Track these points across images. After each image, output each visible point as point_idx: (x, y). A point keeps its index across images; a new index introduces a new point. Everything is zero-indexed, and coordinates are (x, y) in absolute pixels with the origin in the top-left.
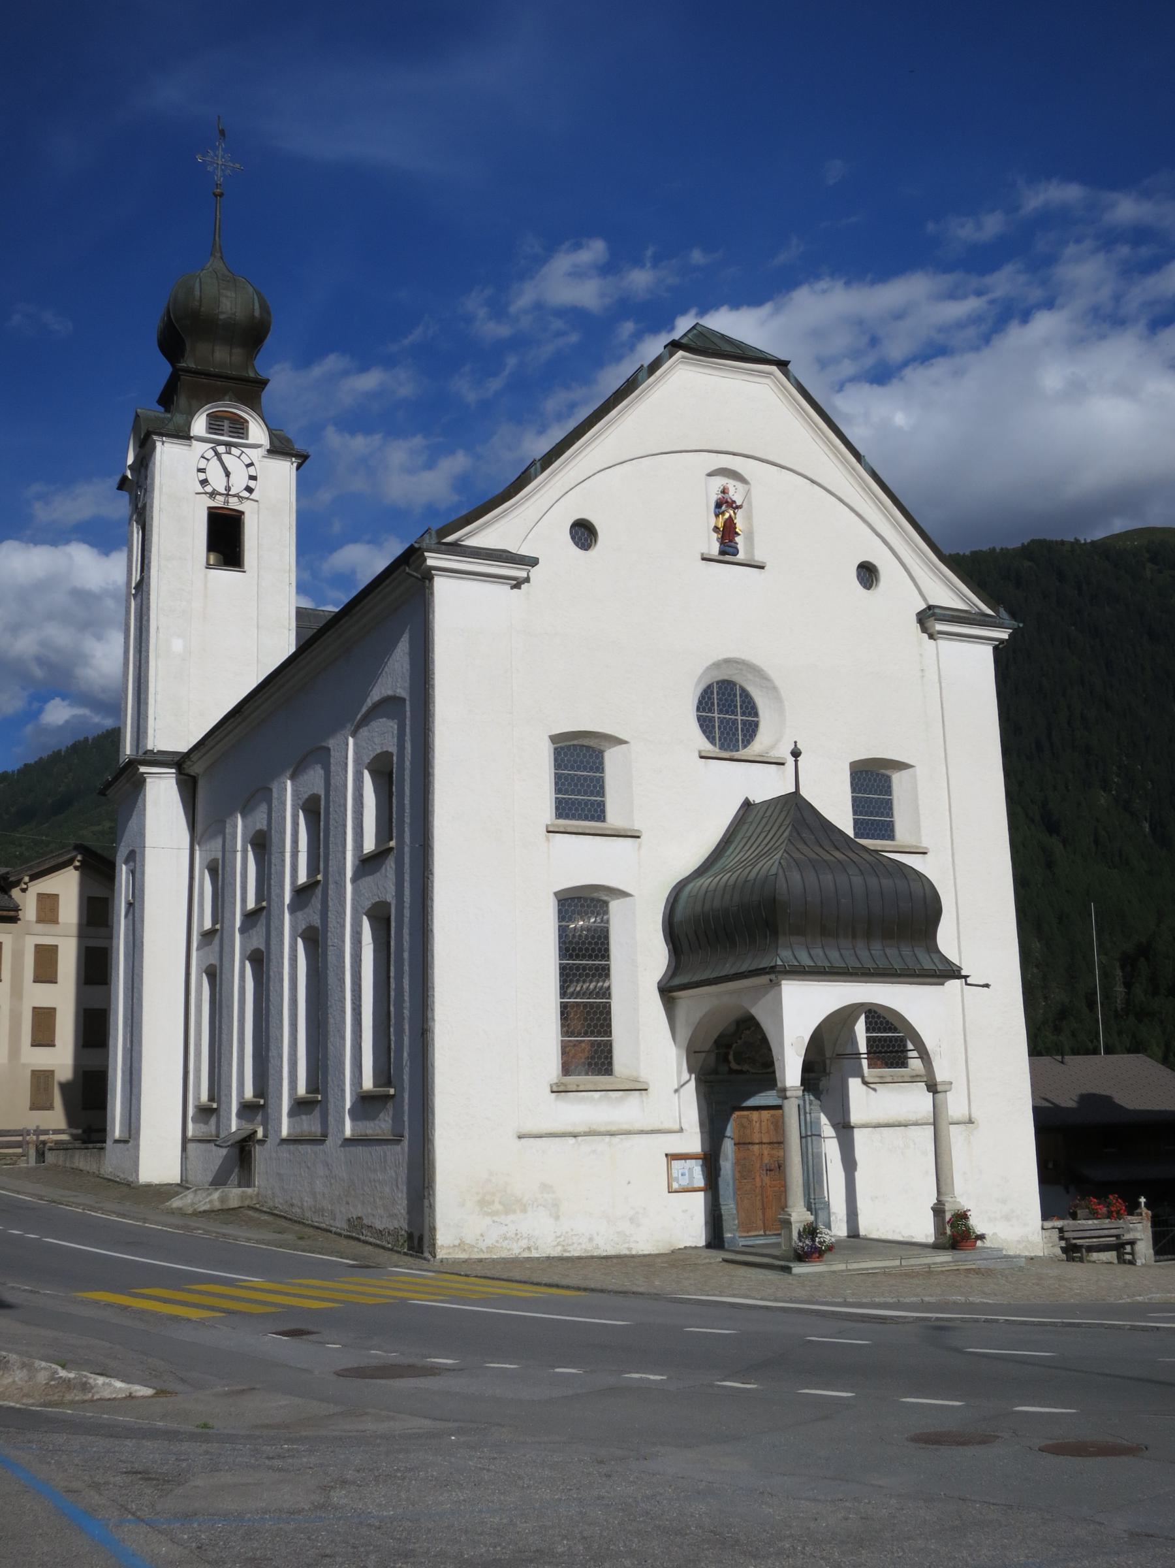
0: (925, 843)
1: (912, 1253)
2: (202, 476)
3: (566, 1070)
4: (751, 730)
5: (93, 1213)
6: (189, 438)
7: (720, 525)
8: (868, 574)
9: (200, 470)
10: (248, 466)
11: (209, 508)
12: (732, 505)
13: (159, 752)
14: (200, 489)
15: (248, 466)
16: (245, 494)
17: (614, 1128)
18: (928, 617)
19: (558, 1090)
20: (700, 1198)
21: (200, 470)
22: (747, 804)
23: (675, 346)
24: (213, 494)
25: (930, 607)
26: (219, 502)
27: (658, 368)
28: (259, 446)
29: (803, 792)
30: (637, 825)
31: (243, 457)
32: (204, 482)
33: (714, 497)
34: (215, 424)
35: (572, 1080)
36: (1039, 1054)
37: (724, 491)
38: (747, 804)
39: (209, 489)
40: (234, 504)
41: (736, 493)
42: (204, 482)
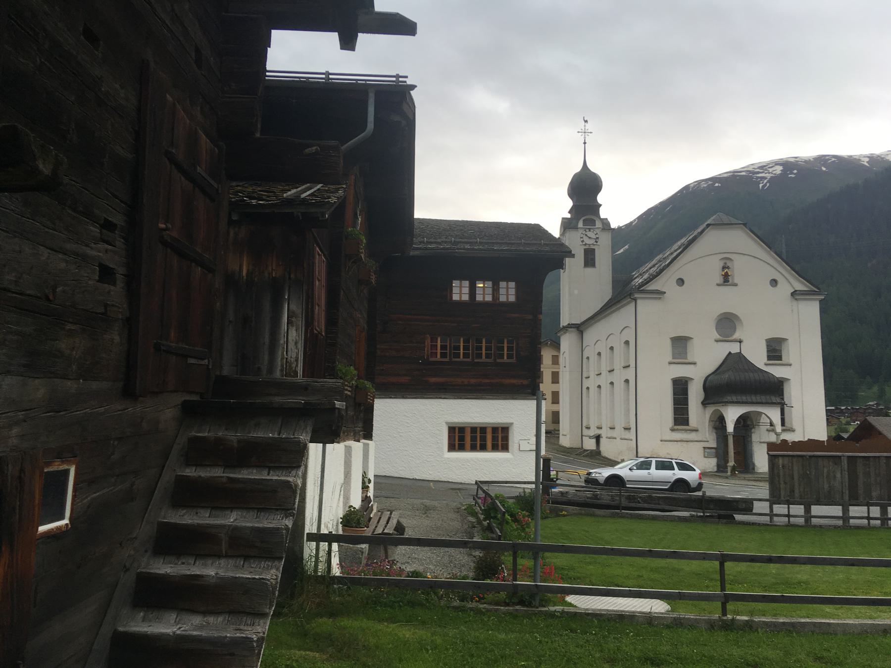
0: (791, 362)
1: (594, 461)
2: (582, 239)
3: (676, 424)
4: (734, 329)
5: (259, 663)
6: (577, 228)
7: (723, 274)
8: (774, 283)
9: (581, 238)
10: (596, 234)
11: (585, 249)
12: (728, 268)
13: (572, 324)
14: (581, 244)
15: (596, 234)
16: (595, 243)
17: (689, 440)
18: (794, 294)
19: (672, 430)
20: (534, 453)
21: (581, 238)
22: (730, 353)
23: (708, 225)
24: (585, 245)
25: (796, 291)
26: (587, 247)
27: (703, 232)
28: (600, 228)
29: (742, 352)
30: (695, 360)
31: (594, 232)
32: (583, 241)
33: (722, 265)
34: (586, 222)
35: (676, 427)
36: (829, 426)
37: (725, 263)
38: (730, 353)
39: (584, 243)
40: (592, 247)
41: (729, 264)
42: (583, 241)
